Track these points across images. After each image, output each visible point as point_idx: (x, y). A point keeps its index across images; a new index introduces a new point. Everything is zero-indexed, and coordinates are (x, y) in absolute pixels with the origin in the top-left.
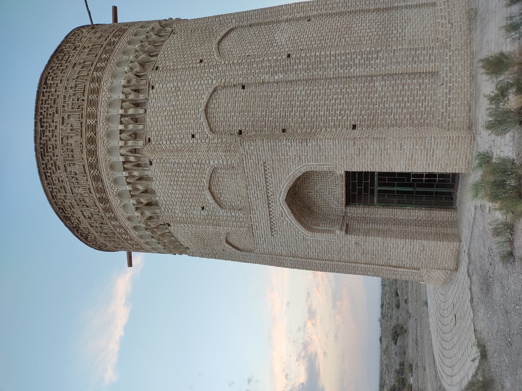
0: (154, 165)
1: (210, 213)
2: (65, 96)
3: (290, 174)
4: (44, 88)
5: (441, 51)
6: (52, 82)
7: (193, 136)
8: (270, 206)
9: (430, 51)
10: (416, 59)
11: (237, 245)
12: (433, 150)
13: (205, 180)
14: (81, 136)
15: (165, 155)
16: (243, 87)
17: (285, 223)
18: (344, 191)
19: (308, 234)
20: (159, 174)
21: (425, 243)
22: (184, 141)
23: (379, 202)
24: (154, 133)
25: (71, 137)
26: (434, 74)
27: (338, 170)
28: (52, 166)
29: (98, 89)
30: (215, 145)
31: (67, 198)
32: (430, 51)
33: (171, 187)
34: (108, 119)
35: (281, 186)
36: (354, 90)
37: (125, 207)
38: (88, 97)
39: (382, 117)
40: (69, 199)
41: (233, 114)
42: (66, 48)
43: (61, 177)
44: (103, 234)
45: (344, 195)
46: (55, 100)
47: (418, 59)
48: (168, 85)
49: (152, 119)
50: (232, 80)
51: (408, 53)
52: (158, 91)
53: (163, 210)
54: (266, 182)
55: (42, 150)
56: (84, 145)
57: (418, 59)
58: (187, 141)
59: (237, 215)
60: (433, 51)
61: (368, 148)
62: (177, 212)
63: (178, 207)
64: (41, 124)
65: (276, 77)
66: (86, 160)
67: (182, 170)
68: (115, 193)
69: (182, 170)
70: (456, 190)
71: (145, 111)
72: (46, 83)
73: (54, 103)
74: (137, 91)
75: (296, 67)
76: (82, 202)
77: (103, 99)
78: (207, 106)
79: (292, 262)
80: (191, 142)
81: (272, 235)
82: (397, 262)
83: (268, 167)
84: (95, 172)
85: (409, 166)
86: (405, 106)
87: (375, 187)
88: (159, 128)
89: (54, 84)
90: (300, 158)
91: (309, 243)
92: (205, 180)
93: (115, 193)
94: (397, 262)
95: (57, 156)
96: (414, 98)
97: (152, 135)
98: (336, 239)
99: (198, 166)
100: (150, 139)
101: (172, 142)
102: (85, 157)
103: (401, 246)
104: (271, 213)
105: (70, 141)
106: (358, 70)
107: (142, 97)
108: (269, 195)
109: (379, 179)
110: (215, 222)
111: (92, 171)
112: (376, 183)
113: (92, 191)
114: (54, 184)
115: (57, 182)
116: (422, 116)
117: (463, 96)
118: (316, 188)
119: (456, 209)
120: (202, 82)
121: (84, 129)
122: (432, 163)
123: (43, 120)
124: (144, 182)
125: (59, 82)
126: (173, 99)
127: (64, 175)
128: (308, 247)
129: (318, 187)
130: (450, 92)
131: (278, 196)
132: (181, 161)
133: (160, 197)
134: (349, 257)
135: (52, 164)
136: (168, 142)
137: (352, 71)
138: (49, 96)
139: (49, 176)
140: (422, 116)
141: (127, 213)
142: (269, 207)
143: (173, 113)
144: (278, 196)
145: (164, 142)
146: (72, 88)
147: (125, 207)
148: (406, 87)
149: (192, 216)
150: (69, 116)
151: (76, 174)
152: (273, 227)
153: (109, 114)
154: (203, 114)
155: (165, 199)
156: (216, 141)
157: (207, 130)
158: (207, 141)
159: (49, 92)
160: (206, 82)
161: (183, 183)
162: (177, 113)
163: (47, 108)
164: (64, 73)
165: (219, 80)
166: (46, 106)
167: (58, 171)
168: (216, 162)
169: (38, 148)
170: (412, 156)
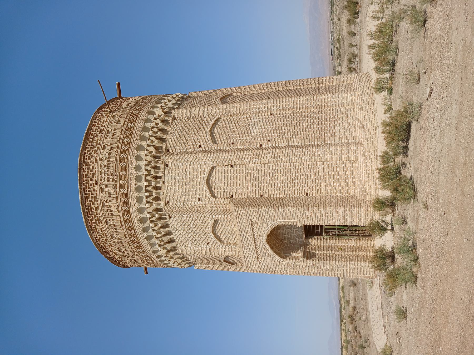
0: (172, 218)
4: (83, 166)
6: (89, 161)
7: (199, 200)
16: (232, 166)
19: (283, 261)
29: (126, 167)
30: (215, 205)
33: (185, 231)
38: (119, 173)
41: (226, 184)
42: (93, 131)
43: (103, 228)
48: (178, 164)
50: (224, 162)
52: (171, 168)
56: (120, 207)
67: (193, 221)
73: (93, 177)
75: (266, 155)
77: (131, 174)
81: (258, 261)
89: (91, 162)
95: (99, 214)
97: (170, 199)
99: (205, 219)
101: (185, 203)
106: (307, 158)
111: (127, 224)
120: (203, 163)
123: (86, 189)
125: (94, 161)
126: (183, 174)
127: (105, 227)
135: (95, 220)
136: (182, 204)
138: (88, 171)
143: (184, 184)
145: (179, 204)
146: (105, 166)
148: (338, 169)
149: (200, 248)
154: (206, 185)
156: (216, 202)
157: (209, 195)
160: (206, 163)
162: (187, 184)
163: (88, 180)
164: (97, 153)
165: (215, 162)
166: (87, 179)
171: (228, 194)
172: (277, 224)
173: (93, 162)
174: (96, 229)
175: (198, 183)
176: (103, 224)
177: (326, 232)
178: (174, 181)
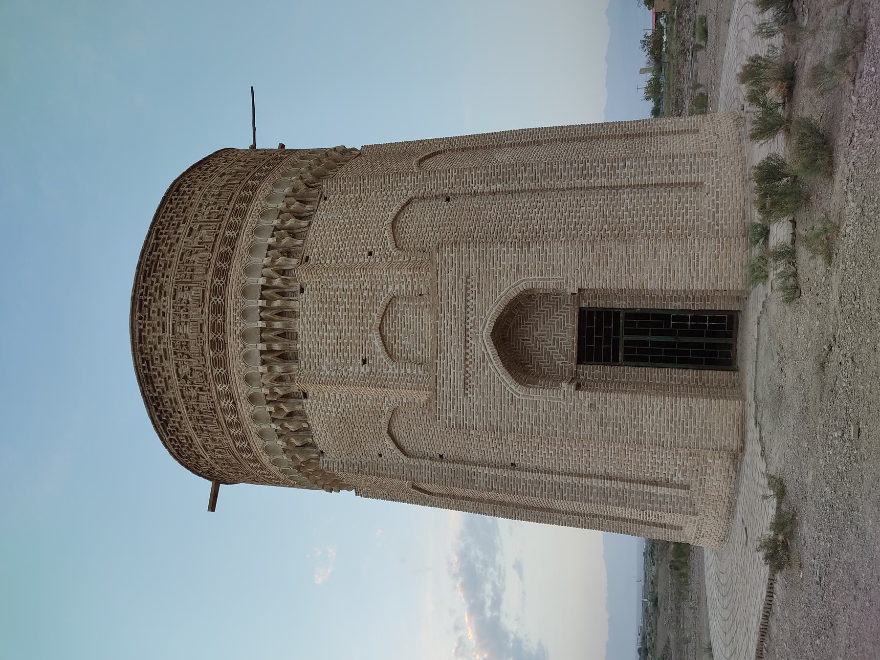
1: (374, 370)
2: (201, 205)
3: (502, 293)
5: (706, 159)
7: (370, 254)
8: (468, 345)
9: (692, 160)
10: (673, 168)
11: (403, 442)
12: (698, 256)
13: (375, 315)
14: (212, 252)
15: (325, 275)
17: (486, 374)
18: (576, 326)
20: (311, 306)
21: (693, 402)
22: (355, 260)
23: (626, 359)
24: (315, 250)
25: (197, 253)
26: (697, 185)
27: (570, 286)
28: (156, 291)
31: (162, 341)
32: (692, 160)
33: (323, 327)
35: (487, 313)
36: (594, 203)
37: (246, 357)
39: (630, 232)
40: (164, 343)
43: (164, 307)
44: (197, 414)
45: (576, 332)
46: (186, 208)
47: (677, 168)
49: (317, 234)
51: (664, 161)
53: (303, 366)
54: (467, 307)
55: (147, 268)
57: (677, 168)
58: (361, 260)
59: (415, 372)
60: (695, 159)
61: (611, 254)
62: (324, 368)
63: (326, 360)
64: (156, 236)
65: (494, 187)
66: (209, 283)
68: (238, 332)
69: (346, 300)
70: (736, 341)
71: (310, 224)
72: (177, 190)
75: (520, 175)
76: (184, 347)
78: (395, 219)
79: (487, 479)
80: (367, 260)
82: (652, 437)
83: (472, 283)
84: (219, 300)
85: (666, 279)
86: (660, 220)
87: (620, 336)
88: (324, 244)
90: (517, 269)
91: (520, 407)
92: (375, 315)
93: (238, 332)
94: (652, 437)
96: (672, 212)
97: (312, 252)
98: (562, 398)
100: (308, 257)
101: (339, 261)
102: (209, 278)
103: (658, 409)
104: (468, 357)
105: (194, 257)
107: (308, 207)
108: (468, 327)
109: (626, 324)
110: (379, 383)
112: (622, 330)
113: (205, 328)
114: (150, 318)
115: (156, 314)
116: (682, 231)
117: (734, 201)
118: (535, 334)
119: (736, 370)
120: (394, 192)
121: (218, 242)
122: (697, 276)
124: (286, 319)
128: (518, 413)
129: (539, 332)
130: (717, 197)
131: (481, 329)
132: (346, 287)
133: (304, 345)
134: (580, 432)
135: (156, 288)
137: (592, 181)
139: (145, 306)
140: (682, 231)
141: (247, 367)
142: (466, 348)
144: (481, 329)
145: (328, 262)
146: (213, 195)
147: (246, 357)
149: (345, 374)
150: (200, 226)
151: (188, 303)
152: (467, 381)
153: (259, 226)
154: (389, 228)
155: (311, 346)
156: (401, 260)
158: (389, 259)
159: (180, 199)
160: (399, 192)
161: (343, 320)
163: (172, 217)
164: (174, 251)
167: (163, 298)
168: (397, 287)
169: (144, 262)
170: (670, 265)
177: (626, 351)
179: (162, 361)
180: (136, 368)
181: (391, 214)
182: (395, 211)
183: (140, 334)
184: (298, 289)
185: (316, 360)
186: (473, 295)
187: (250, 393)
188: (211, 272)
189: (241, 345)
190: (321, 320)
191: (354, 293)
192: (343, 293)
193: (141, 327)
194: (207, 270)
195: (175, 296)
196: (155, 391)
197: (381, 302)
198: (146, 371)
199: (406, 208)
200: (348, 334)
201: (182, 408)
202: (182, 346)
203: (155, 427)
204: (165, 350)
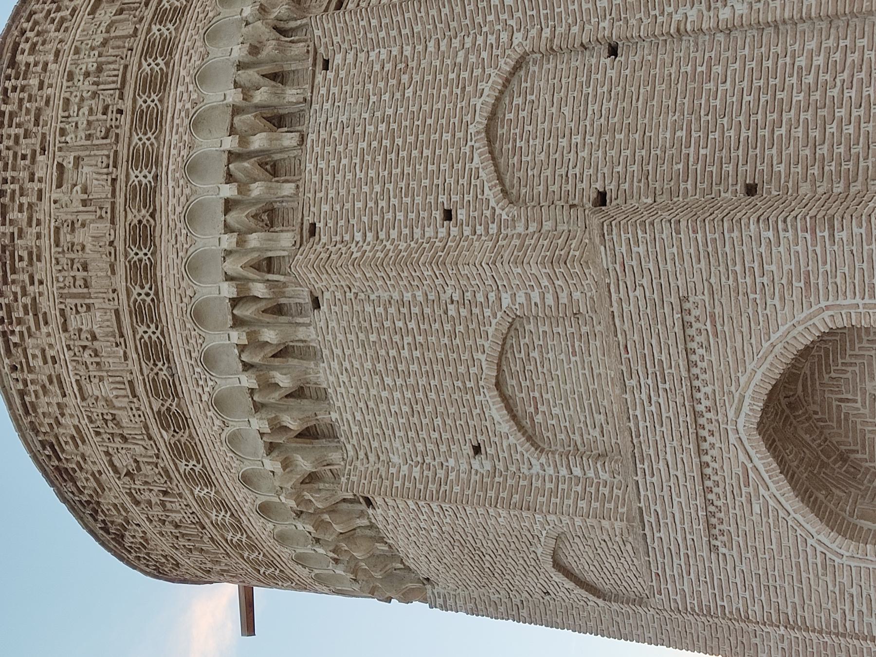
2: (67, 101)
3: (774, 337)
7: (448, 215)
13: (483, 357)
16: (613, 51)
17: (756, 509)
20: (340, 337)
22: (418, 232)
25: (83, 225)
28: (26, 313)
29: (165, 75)
31: (67, 411)
33: (376, 379)
34: (192, 168)
35: (743, 380)
38: (134, 101)
40: (72, 416)
43: (51, 346)
44: (169, 528)
46: (39, 111)
50: (575, 29)
52: (342, 74)
53: (351, 453)
54: (690, 365)
56: (120, 246)
58: (429, 232)
59: (591, 474)
62: (395, 459)
63: (397, 444)
66: (123, 296)
68: (205, 398)
69: (412, 325)
71: (303, 139)
73: (37, 123)
74: (278, 77)
76: (110, 424)
77: (179, 106)
78: (493, 117)
79: (786, 645)
83: (695, 312)
88: (343, 192)
90: (808, 283)
91: (846, 580)
92: (483, 357)
93: (205, 398)
97: (321, 212)
100: (313, 225)
101: (382, 235)
104: (708, 471)
105: (80, 236)
107: (292, 94)
108: (700, 408)
110: (516, 498)
111: (141, 329)
113: (140, 390)
114: (31, 370)
115: (40, 361)
120: (480, 40)
121: (120, 200)
125: (51, 57)
127: (60, 340)
128: (842, 593)
131: (731, 414)
132: (408, 296)
133: (342, 412)
135: (25, 307)
136: (370, 236)
139: (16, 345)
141: (241, 460)
142: (700, 452)
143: (386, 143)
144: (731, 414)
145: (358, 236)
149: (441, 473)
150: (77, 159)
151: (94, 338)
152: (713, 521)
153: (196, 153)
154: (481, 145)
155: (359, 417)
156: (520, 229)
157: (492, 194)
160: (492, 39)
161: (414, 367)
162: (399, 141)
164: (39, 223)
165: (533, 32)
166: (13, 131)
167: (44, 330)
168: (521, 298)
171: (585, 185)
172: (822, 324)
173: (46, 64)
174: (25, 350)
175: (447, 137)
176: (53, 325)
178: (348, 131)
179: (77, 446)
180: (35, 458)
181: (483, 103)
182: (489, 90)
183: (23, 399)
184: (308, 300)
185: (375, 444)
186: (702, 339)
187: (258, 502)
188: (121, 270)
189: (217, 422)
190: (368, 365)
191: (427, 311)
192: (404, 310)
193: (20, 386)
194: (112, 267)
195: (65, 323)
196: (81, 493)
197: (491, 331)
198: (56, 463)
199: (515, 81)
200: (432, 395)
201: (141, 518)
202: (106, 421)
203: (103, 544)
204: (76, 428)
